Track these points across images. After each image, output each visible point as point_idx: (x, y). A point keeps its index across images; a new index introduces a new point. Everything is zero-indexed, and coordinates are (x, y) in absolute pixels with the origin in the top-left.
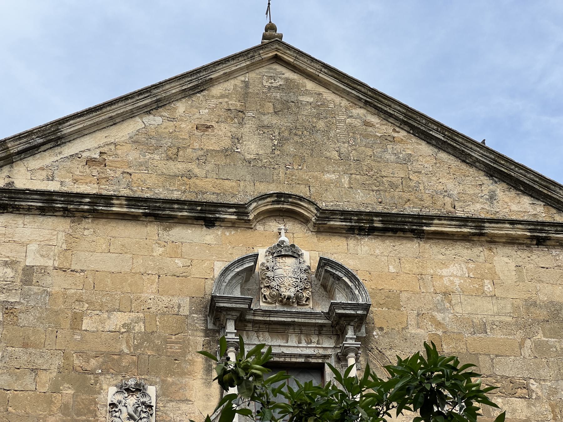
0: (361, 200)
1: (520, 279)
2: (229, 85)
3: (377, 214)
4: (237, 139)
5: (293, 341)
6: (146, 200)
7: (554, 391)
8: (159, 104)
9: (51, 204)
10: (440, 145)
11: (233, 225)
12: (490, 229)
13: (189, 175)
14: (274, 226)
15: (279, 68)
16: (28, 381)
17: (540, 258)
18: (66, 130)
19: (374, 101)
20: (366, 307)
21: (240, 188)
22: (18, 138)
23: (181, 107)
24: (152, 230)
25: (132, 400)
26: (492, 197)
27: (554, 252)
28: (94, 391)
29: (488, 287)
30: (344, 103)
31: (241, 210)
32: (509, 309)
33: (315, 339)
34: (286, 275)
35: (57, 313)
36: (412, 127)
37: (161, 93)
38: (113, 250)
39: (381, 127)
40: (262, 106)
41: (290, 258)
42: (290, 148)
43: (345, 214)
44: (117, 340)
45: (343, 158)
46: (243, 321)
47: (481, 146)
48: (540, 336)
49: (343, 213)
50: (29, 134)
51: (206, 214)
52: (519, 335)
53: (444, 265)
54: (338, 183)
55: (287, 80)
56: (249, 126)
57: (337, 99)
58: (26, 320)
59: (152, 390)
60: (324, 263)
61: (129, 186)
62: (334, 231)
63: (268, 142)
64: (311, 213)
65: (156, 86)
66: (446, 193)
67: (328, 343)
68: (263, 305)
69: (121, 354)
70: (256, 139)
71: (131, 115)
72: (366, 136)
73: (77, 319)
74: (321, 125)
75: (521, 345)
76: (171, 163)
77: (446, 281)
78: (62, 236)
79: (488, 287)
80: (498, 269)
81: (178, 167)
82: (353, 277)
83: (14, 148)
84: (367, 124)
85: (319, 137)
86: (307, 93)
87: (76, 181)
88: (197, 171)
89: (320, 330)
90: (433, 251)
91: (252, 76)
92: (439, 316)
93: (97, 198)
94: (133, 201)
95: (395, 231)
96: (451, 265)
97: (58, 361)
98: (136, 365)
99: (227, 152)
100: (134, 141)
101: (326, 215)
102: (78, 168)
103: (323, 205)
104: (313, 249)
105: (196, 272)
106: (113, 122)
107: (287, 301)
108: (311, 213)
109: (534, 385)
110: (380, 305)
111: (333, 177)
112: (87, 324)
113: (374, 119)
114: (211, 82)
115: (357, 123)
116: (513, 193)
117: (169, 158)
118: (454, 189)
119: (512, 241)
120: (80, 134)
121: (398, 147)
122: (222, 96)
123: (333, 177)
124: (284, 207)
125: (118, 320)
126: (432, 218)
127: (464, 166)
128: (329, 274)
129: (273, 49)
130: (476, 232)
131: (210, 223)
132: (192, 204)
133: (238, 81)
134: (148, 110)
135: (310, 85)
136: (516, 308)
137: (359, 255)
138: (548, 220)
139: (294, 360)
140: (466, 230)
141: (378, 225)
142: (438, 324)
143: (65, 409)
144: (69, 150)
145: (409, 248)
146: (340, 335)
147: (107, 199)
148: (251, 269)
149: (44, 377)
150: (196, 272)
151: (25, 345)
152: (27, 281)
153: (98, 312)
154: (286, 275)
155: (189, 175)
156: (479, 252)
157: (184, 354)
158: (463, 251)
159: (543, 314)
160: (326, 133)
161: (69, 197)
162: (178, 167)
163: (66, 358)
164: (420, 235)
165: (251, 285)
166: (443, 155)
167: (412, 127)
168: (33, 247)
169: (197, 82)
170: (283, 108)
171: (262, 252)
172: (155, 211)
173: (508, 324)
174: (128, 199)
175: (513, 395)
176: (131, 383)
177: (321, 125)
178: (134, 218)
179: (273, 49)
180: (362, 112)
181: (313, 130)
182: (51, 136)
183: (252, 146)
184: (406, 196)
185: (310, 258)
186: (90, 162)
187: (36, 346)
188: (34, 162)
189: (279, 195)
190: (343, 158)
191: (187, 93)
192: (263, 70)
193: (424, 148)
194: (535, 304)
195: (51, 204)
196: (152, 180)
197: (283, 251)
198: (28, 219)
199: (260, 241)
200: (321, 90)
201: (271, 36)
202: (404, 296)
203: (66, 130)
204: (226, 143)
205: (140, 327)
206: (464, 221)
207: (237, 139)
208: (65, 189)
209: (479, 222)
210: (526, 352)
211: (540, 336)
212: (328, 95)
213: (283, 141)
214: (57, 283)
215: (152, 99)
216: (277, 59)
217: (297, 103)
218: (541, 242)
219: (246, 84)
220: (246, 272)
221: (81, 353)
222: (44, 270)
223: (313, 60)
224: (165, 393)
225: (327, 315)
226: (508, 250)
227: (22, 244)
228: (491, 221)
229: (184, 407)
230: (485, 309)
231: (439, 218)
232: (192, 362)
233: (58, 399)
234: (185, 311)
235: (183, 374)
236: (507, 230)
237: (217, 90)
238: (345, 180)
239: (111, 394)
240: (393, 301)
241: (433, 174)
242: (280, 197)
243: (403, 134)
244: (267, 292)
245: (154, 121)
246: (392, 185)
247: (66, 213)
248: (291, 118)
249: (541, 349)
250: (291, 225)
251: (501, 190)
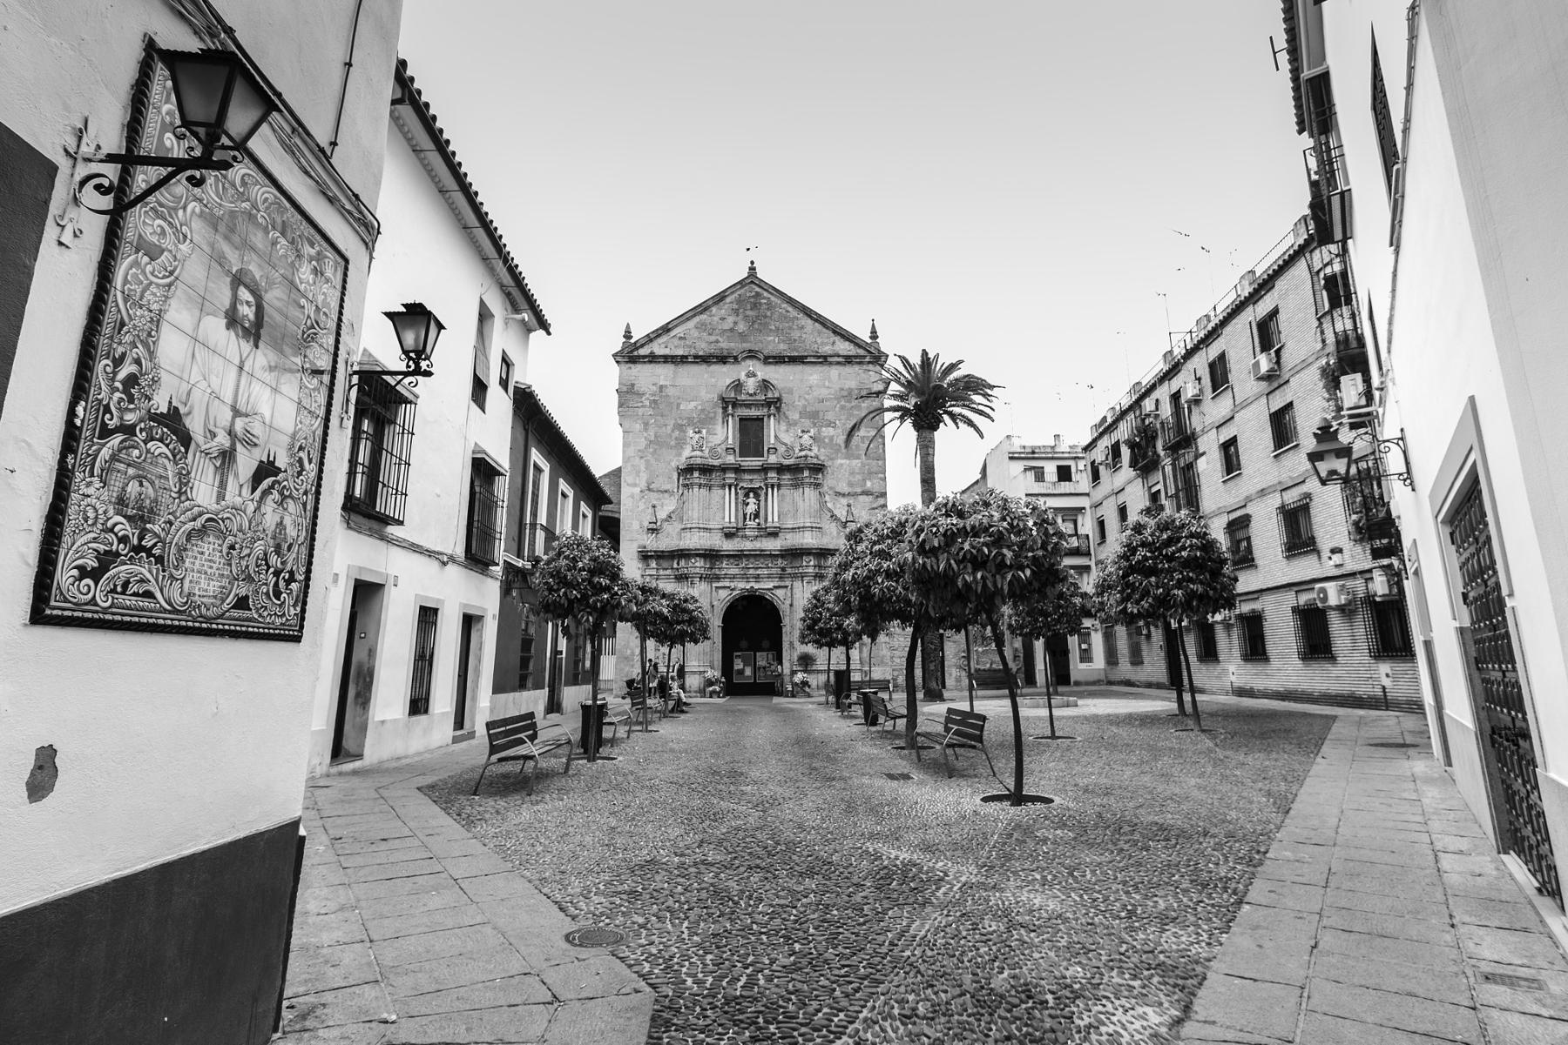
9: (667, 359)
21: (735, 346)
24: (704, 367)
31: (736, 358)
46: (735, 405)
51: (722, 359)
73: (678, 405)
81: (713, 338)
90: (808, 369)
96: (813, 376)
99: (732, 330)
101: (766, 358)
102: (676, 341)
119: (838, 363)
124: (752, 355)
128: (765, 385)
130: (824, 360)
139: (1185, 673)
144: (672, 333)
145: (799, 368)
153: (1209, 467)
154: (751, 385)
156: (825, 368)
158: (819, 368)
161: (673, 357)
170: (755, 306)
172: (704, 359)
183: (741, 327)
191: (716, 303)
193: (810, 321)
195: (667, 359)
196: (704, 345)
197: (751, 375)
199: (739, 372)
230: (824, 393)
240: (790, 392)
245: (703, 317)
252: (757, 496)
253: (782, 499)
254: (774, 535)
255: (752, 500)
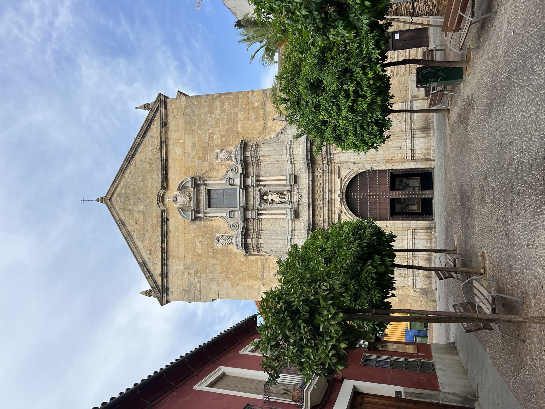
0: (157, 176)
1: (178, 131)
2: (121, 214)
3: (162, 172)
4: (139, 212)
5: (201, 197)
6: (162, 238)
7: (211, 126)
8: (129, 235)
9: (165, 264)
10: (136, 151)
11: (167, 213)
12: (163, 139)
13: (152, 226)
14: (167, 201)
15: (113, 199)
16: (217, 266)
17: (171, 124)
18: (141, 261)
19: (123, 170)
20: (192, 178)
21: (156, 211)
22: (145, 274)
23: (130, 228)
24: (170, 236)
25: (221, 240)
26: (152, 137)
27: (169, 120)
28: (218, 250)
29: (181, 141)
30: (124, 179)
31: (163, 211)
32: (188, 136)
33: (201, 191)
34: (183, 199)
35: (197, 260)
36: (131, 159)
37: (126, 234)
38: (177, 246)
39: (131, 168)
40: (127, 204)
41: (176, 200)
42: (141, 196)
43: (162, 182)
44: (204, 244)
45: (143, 180)
46: (197, 212)
47: (136, 139)
48: (196, 128)
49: (162, 182)
50: (143, 271)
51: (165, 221)
52: (195, 134)
53: (176, 153)
54: (151, 183)
55: (117, 196)
56: (134, 208)
57: (122, 181)
58: (199, 268)
59: (218, 235)
60: (179, 189)
61: (157, 243)
62: (167, 185)
63: (140, 203)
64: (162, 192)
65: (124, 236)
66: (152, 150)
67: (202, 188)
68: (192, 205)
69: (208, 243)
70: (139, 206)
71: (134, 243)
72: (135, 174)
73: (199, 255)
74: (132, 187)
75: (199, 134)
76: (149, 231)
77: (180, 153)
78: (174, 260)
79: (181, 141)
80: (175, 137)
81: (150, 229)
82: (183, 182)
83: (148, 275)
84: (130, 173)
85: (136, 188)
86: (121, 190)
87: (157, 257)
88: (151, 223)
89: (198, 190)
90: (171, 156)
91: (116, 207)
92: (192, 156)
93: (163, 252)
94: (163, 242)
95: (166, 167)
97: (211, 259)
98: (211, 239)
99: (144, 215)
100: (142, 241)
101: (163, 187)
102: (153, 257)
103: (160, 188)
104: (173, 191)
105: (183, 224)
106: (137, 248)
107: (190, 199)
108: (162, 192)
109: (210, 132)
110: (189, 173)
111: (149, 184)
112: (200, 252)
113: (129, 171)
114: (120, 220)
115: (130, 176)
116: (150, 130)
117: (147, 231)
118: (150, 148)
119: (166, 132)
120: (141, 257)
121: (137, 164)
122: (125, 216)
123: (149, 184)
124: (161, 199)
125: (198, 244)
126: (161, 157)
127: (142, 144)
128: (182, 188)
129: (107, 200)
130: (164, 144)
131: (167, 220)
132: (162, 225)
133: (119, 212)
134: (132, 238)
135: (118, 189)
136: (187, 134)
137: (175, 180)
138: (159, 120)
140: (164, 146)
141: (165, 172)
142: (194, 157)
143: (223, 257)
144: (147, 260)
145: (171, 163)
146: (199, 185)
147: (163, 249)
148: (182, 209)
149: (215, 262)
150: (183, 224)
151: (207, 268)
152: (188, 268)
155: (152, 226)
156: (171, 143)
157: (207, 227)
158: (170, 147)
159: (188, 126)
160: (135, 186)
161: (163, 259)
162: (150, 229)
163: (209, 257)
164: (166, 160)
165: (186, 208)
166: (139, 150)
167: (131, 159)
168: (178, 268)
169: (121, 224)
170: (127, 198)
171: (175, 205)
172: (165, 235)
173: (192, 137)
174: (162, 243)
175: (213, 138)
176: (216, 241)
177: (132, 187)
178: (167, 241)
179: (107, 200)
180: (126, 174)
181: (134, 189)
182: (143, 265)
184: (154, 163)
185: (176, 192)
186: (150, 253)
187: (207, 265)
188: (152, 269)
189: (158, 200)
190: (143, 180)
191: (125, 226)
192: (114, 203)
193: (137, 156)
194: (186, 128)
195: (165, 264)
198: (169, 269)
199: (173, 207)
200: (120, 186)
201: (102, 200)
202: (186, 166)
203: (141, 261)
204: (141, 215)
205: (200, 238)
206: (162, 147)
207: (139, 212)
208: (160, 260)
209: (162, 142)
210: (200, 132)
211: (196, 128)
212: (121, 184)
213: (138, 198)
214: (188, 261)
215: (128, 237)
216: (110, 200)
217: (125, 193)
218: (166, 124)
219: (120, 209)
220: (183, 210)
221: (208, 253)
222: (185, 264)
223: (110, 189)
224: (218, 232)
225: (194, 188)
226: (169, 133)
227: (177, 270)
228: (161, 139)
229: (222, 226)
230: (188, 143)
231: (161, 154)
232: (209, 225)
233: (221, 258)
234: (195, 227)
235: (213, 227)
236: (163, 134)
237: (123, 218)
238: (150, 180)
239: (219, 246)
240: (188, 169)
241: (146, 154)
242: (158, 200)
243: (133, 162)
244: (188, 205)
245: (135, 236)
246: (151, 166)
247: (167, 259)
248: (130, 196)
249: (199, 128)
250: (166, 197)
251: (149, 134)
252: (266, 194)
253: (269, 173)
254: (296, 179)
255: (270, 197)
